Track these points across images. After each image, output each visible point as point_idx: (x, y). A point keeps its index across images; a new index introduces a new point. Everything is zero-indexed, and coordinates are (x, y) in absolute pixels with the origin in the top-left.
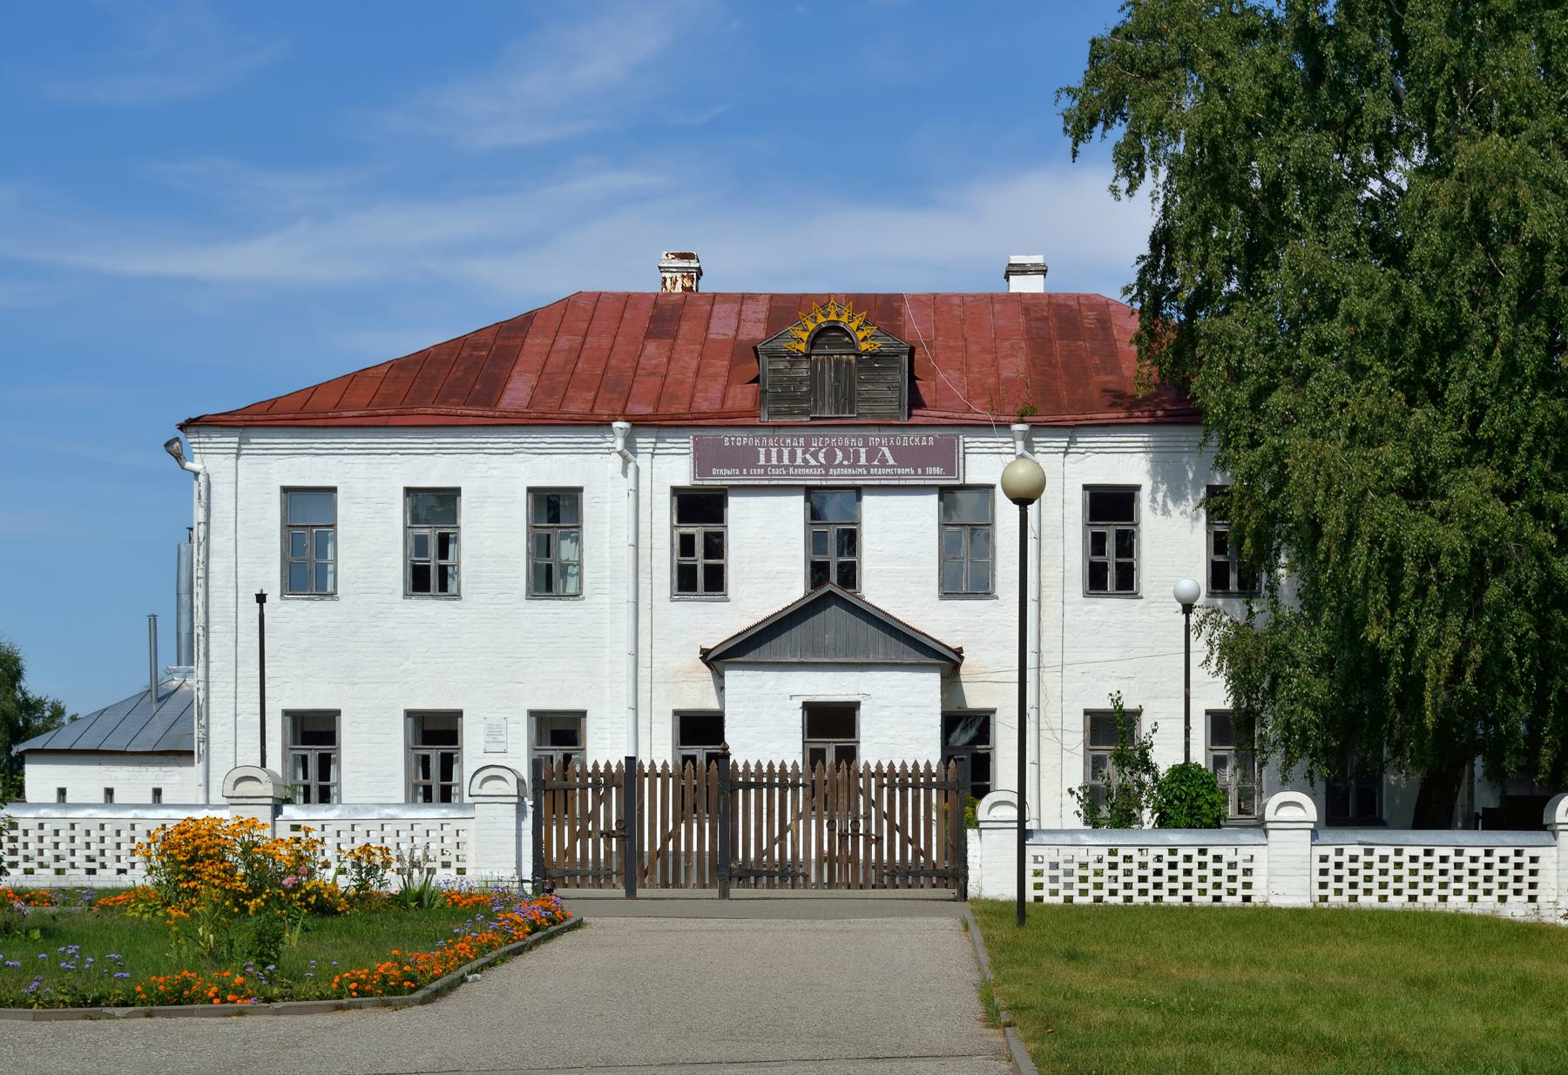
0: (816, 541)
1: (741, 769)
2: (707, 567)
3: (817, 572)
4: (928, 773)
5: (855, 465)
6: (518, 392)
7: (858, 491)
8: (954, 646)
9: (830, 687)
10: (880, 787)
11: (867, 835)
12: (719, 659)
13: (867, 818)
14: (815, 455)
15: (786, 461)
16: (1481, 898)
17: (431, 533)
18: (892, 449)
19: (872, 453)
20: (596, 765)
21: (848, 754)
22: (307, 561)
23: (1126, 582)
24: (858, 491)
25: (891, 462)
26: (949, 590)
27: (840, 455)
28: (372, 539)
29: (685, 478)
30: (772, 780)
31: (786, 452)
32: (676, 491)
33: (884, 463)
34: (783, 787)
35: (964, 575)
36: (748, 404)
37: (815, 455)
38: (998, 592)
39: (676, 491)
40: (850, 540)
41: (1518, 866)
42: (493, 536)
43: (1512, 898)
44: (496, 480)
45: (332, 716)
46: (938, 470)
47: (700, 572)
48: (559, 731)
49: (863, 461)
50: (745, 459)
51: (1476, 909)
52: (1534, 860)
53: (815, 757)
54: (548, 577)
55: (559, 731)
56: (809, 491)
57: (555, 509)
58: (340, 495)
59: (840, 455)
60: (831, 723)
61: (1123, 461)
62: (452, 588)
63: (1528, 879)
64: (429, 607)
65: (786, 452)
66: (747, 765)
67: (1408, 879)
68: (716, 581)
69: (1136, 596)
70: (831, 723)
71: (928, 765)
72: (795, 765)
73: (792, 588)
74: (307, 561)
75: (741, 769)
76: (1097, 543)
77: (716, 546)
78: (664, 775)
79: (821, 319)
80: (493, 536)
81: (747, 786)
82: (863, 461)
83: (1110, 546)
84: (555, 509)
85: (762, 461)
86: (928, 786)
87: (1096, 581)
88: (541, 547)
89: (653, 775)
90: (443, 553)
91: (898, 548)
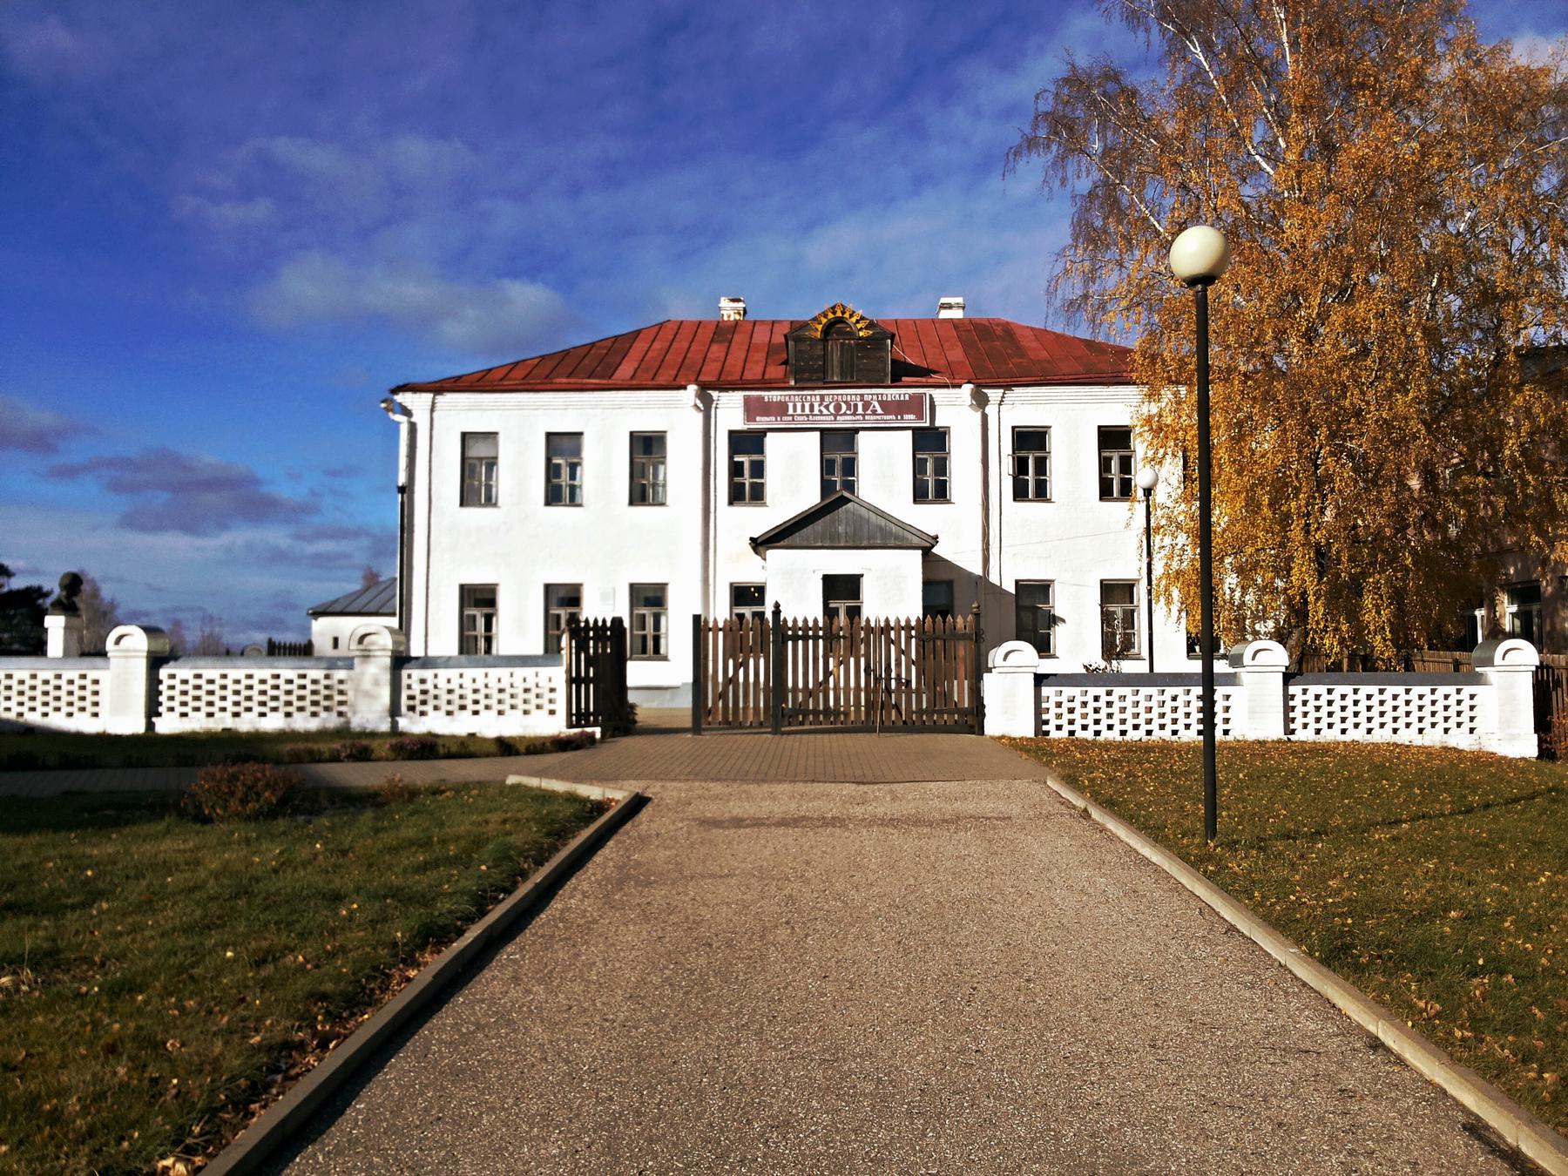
0: (827, 467)
1: (790, 624)
2: (752, 484)
3: (826, 487)
4: (806, 627)
5: (854, 414)
6: (625, 370)
7: (857, 430)
8: (932, 534)
9: (842, 562)
10: (909, 638)
11: (899, 677)
12: (760, 544)
13: (898, 664)
14: (827, 407)
15: (807, 411)
16: (191, 714)
17: (839, 458)
18: (881, 403)
19: (866, 405)
20: (587, 621)
21: (854, 612)
22: (476, 485)
23: (1042, 494)
24: (857, 430)
25: (880, 411)
26: (920, 496)
27: (844, 407)
28: (520, 470)
29: (739, 424)
30: (804, 633)
31: (807, 406)
32: (732, 433)
33: (874, 413)
34: (805, 638)
35: (931, 486)
36: (781, 375)
37: (827, 407)
38: (585, 502)
39: (732, 433)
40: (850, 467)
41: (58, 688)
42: (604, 468)
43: (1428, 729)
44: (605, 420)
45: (662, 588)
46: (912, 417)
47: (747, 488)
48: (563, 597)
49: (860, 411)
50: (781, 409)
51: (1418, 741)
52: (96, 682)
53: (830, 613)
54: (643, 492)
55: (563, 597)
56: (822, 431)
57: (647, 447)
58: (501, 438)
59: (844, 407)
60: (841, 588)
61: (1119, 405)
62: (578, 501)
63: (90, 699)
64: (560, 513)
65: (807, 406)
66: (795, 621)
67: (62, 693)
68: (758, 495)
69: (949, 502)
70: (841, 588)
71: (816, 621)
72: (816, 621)
73: (809, 496)
74: (476, 485)
75: (790, 624)
76: (1104, 465)
77: (758, 469)
78: (908, 627)
79: (831, 316)
80: (604, 468)
81: (795, 638)
82: (860, 411)
83: (1115, 465)
84: (647, 447)
85: (791, 411)
86: (816, 638)
87: (1020, 493)
88: (552, 471)
89: (716, 629)
90: (573, 476)
91: (884, 467)
